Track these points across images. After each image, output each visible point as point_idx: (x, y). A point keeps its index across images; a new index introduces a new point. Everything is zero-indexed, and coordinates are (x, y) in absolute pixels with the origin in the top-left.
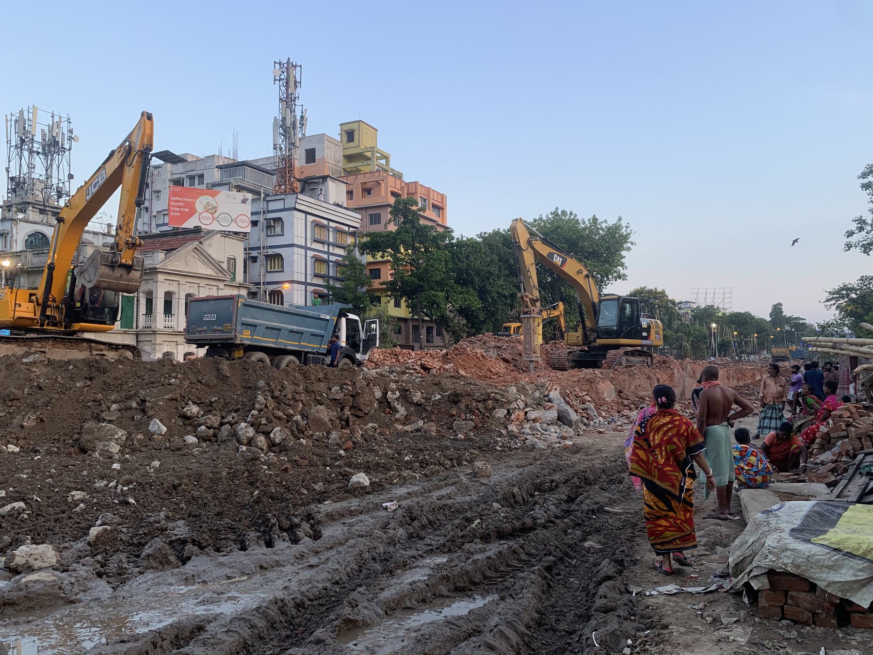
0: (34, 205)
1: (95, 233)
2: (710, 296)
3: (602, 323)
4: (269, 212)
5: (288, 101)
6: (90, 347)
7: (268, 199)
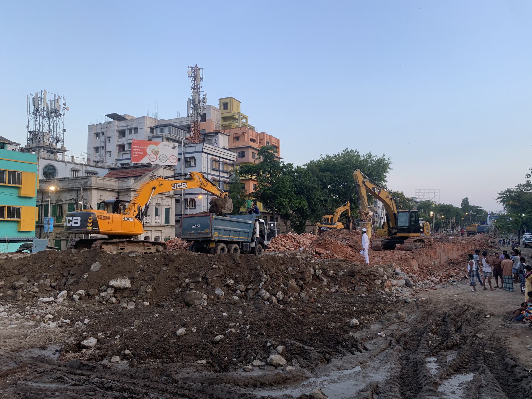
0: (44, 148)
1: (81, 165)
2: (426, 194)
3: (400, 224)
4: (187, 153)
5: (196, 88)
6: (144, 245)
7: (186, 146)
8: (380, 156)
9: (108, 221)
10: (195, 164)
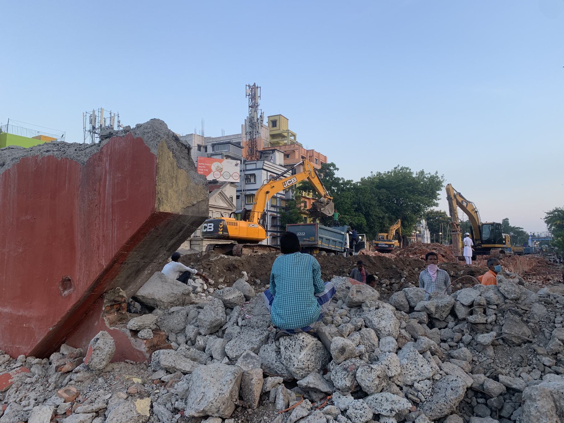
5: (254, 106)
7: (246, 163)
8: (433, 173)
9: (236, 227)
10: (255, 180)
